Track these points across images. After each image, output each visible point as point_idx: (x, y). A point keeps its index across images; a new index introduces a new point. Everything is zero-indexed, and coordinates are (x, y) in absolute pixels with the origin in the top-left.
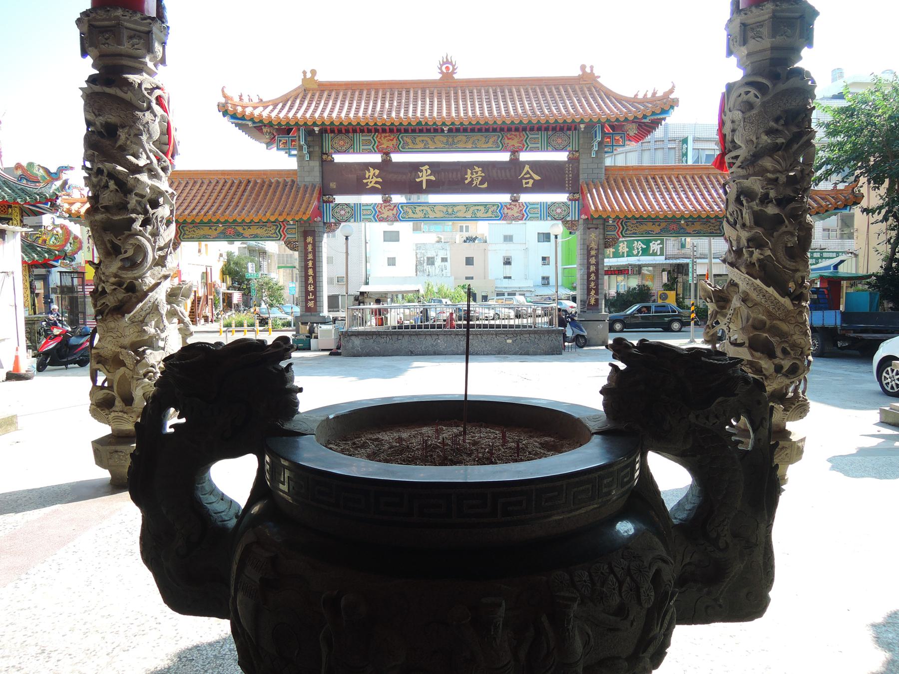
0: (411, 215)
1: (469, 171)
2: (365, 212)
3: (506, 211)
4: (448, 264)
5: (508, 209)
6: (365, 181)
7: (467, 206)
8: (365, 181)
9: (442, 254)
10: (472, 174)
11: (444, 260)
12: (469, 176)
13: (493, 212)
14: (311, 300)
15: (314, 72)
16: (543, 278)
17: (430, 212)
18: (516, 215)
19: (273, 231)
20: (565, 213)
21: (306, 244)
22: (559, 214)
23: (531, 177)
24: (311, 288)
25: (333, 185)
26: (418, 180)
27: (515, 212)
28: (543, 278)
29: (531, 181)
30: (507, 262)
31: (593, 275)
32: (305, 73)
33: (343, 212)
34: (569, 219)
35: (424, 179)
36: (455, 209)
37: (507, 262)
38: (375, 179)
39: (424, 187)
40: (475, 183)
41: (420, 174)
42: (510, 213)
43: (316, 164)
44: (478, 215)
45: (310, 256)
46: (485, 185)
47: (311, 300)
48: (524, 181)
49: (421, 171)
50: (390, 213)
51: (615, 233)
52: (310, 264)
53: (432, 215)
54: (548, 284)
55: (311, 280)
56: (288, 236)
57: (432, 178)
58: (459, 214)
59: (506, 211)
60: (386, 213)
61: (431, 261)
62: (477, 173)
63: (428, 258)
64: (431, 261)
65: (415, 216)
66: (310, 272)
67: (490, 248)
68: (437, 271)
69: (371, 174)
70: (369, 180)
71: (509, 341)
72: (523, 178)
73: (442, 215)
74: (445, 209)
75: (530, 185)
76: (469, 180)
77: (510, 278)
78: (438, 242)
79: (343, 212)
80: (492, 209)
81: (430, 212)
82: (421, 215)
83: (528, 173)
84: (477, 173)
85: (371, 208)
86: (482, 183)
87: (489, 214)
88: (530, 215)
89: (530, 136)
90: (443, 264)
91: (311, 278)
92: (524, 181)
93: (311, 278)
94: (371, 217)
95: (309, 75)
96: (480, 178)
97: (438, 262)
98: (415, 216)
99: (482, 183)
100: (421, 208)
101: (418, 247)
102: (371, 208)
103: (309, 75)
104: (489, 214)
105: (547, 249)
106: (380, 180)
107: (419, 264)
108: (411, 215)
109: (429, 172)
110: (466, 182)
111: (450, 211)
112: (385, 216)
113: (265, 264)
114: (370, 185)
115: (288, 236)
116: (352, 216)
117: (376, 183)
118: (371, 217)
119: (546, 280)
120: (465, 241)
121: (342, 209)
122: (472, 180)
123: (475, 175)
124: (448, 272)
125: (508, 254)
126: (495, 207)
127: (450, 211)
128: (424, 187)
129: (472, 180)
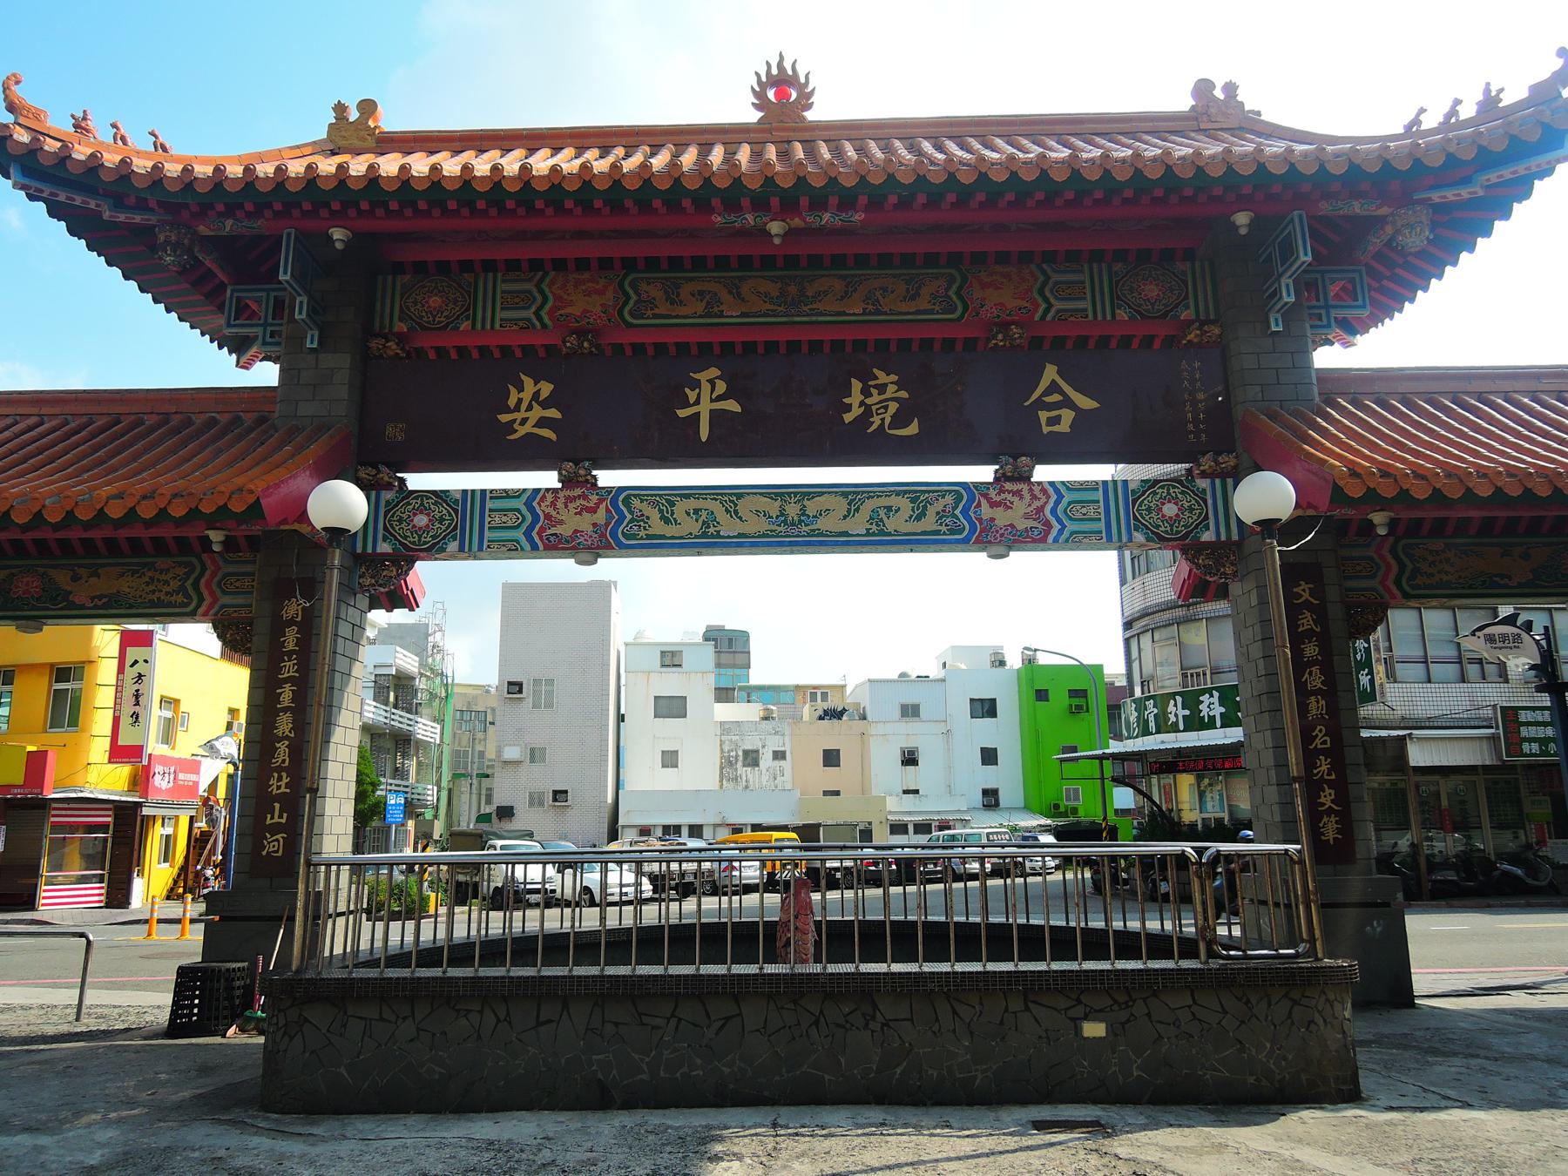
0: (657, 526)
1: (856, 386)
2: (510, 520)
3: (986, 511)
4: (786, 764)
5: (993, 504)
6: (504, 418)
7: (853, 495)
8: (504, 418)
9: (774, 744)
10: (866, 392)
11: (779, 755)
12: (855, 399)
13: (940, 515)
14: (275, 829)
15: (368, 107)
16: (986, 792)
17: (721, 515)
18: (1022, 525)
19: (175, 584)
20: (1190, 519)
21: (279, 626)
22: (1172, 521)
23: (1068, 403)
24: (279, 785)
25: (394, 432)
26: (682, 413)
27: (1017, 514)
28: (986, 792)
29: (1068, 416)
30: (910, 759)
31: (1320, 731)
32: (340, 109)
33: (421, 520)
34: (1207, 537)
35: (705, 409)
36: (812, 507)
37: (910, 759)
38: (538, 412)
39: (704, 434)
40: (876, 420)
41: (692, 396)
42: (1002, 517)
43: (341, 363)
44: (891, 525)
45: (289, 668)
46: (913, 429)
47: (275, 829)
48: (1043, 416)
49: (696, 385)
50: (585, 523)
51: (1375, 583)
52: (286, 695)
53: (728, 527)
54: (997, 804)
55: (282, 753)
56: (226, 600)
57: (732, 406)
58: (822, 524)
59: (986, 511)
60: (571, 522)
61: (752, 758)
62: (882, 388)
63: (746, 753)
64: (752, 758)
65: (670, 530)
66: (284, 725)
67: (873, 730)
68: (764, 779)
69: (527, 395)
70: (519, 416)
71: (1094, 1030)
72: (1040, 404)
73: (764, 525)
74: (774, 507)
75: (1064, 427)
76: (857, 411)
77: (917, 792)
78: (766, 718)
79: (421, 520)
80: (939, 506)
81: (721, 515)
82: (691, 526)
83: (1053, 388)
84: (882, 388)
85: (519, 504)
86: (900, 420)
87: (929, 523)
88: (1071, 527)
89: (1056, 277)
90: (777, 763)
91: (282, 747)
92: (1043, 416)
93: (282, 747)
94: (519, 534)
95: (354, 115)
96: (893, 407)
97: (766, 760)
98: (670, 530)
99: (900, 420)
100: (692, 504)
101: (726, 728)
102: (519, 504)
103: (354, 115)
104: (929, 523)
105: (986, 732)
106: (553, 413)
107: (727, 763)
108: (657, 526)
109: (721, 387)
110: (848, 418)
111: (793, 511)
112: (565, 531)
113: (412, 765)
114: (522, 431)
115: (226, 600)
116: (451, 533)
117: (542, 422)
118: (519, 534)
119: (991, 799)
120: (821, 718)
121: (422, 509)
122: (868, 413)
123: (876, 397)
124: (786, 780)
125: (910, 744)
126: (949, 499)
127: (793, 511)
128: (704, 434)
129: (868, 413)
